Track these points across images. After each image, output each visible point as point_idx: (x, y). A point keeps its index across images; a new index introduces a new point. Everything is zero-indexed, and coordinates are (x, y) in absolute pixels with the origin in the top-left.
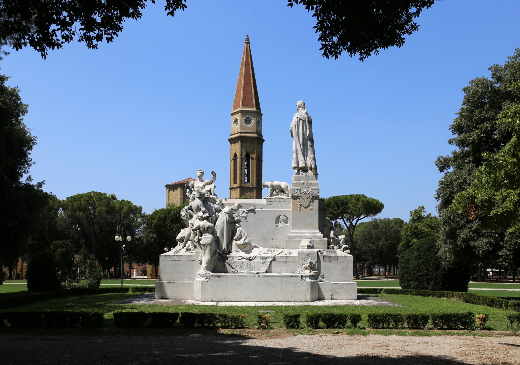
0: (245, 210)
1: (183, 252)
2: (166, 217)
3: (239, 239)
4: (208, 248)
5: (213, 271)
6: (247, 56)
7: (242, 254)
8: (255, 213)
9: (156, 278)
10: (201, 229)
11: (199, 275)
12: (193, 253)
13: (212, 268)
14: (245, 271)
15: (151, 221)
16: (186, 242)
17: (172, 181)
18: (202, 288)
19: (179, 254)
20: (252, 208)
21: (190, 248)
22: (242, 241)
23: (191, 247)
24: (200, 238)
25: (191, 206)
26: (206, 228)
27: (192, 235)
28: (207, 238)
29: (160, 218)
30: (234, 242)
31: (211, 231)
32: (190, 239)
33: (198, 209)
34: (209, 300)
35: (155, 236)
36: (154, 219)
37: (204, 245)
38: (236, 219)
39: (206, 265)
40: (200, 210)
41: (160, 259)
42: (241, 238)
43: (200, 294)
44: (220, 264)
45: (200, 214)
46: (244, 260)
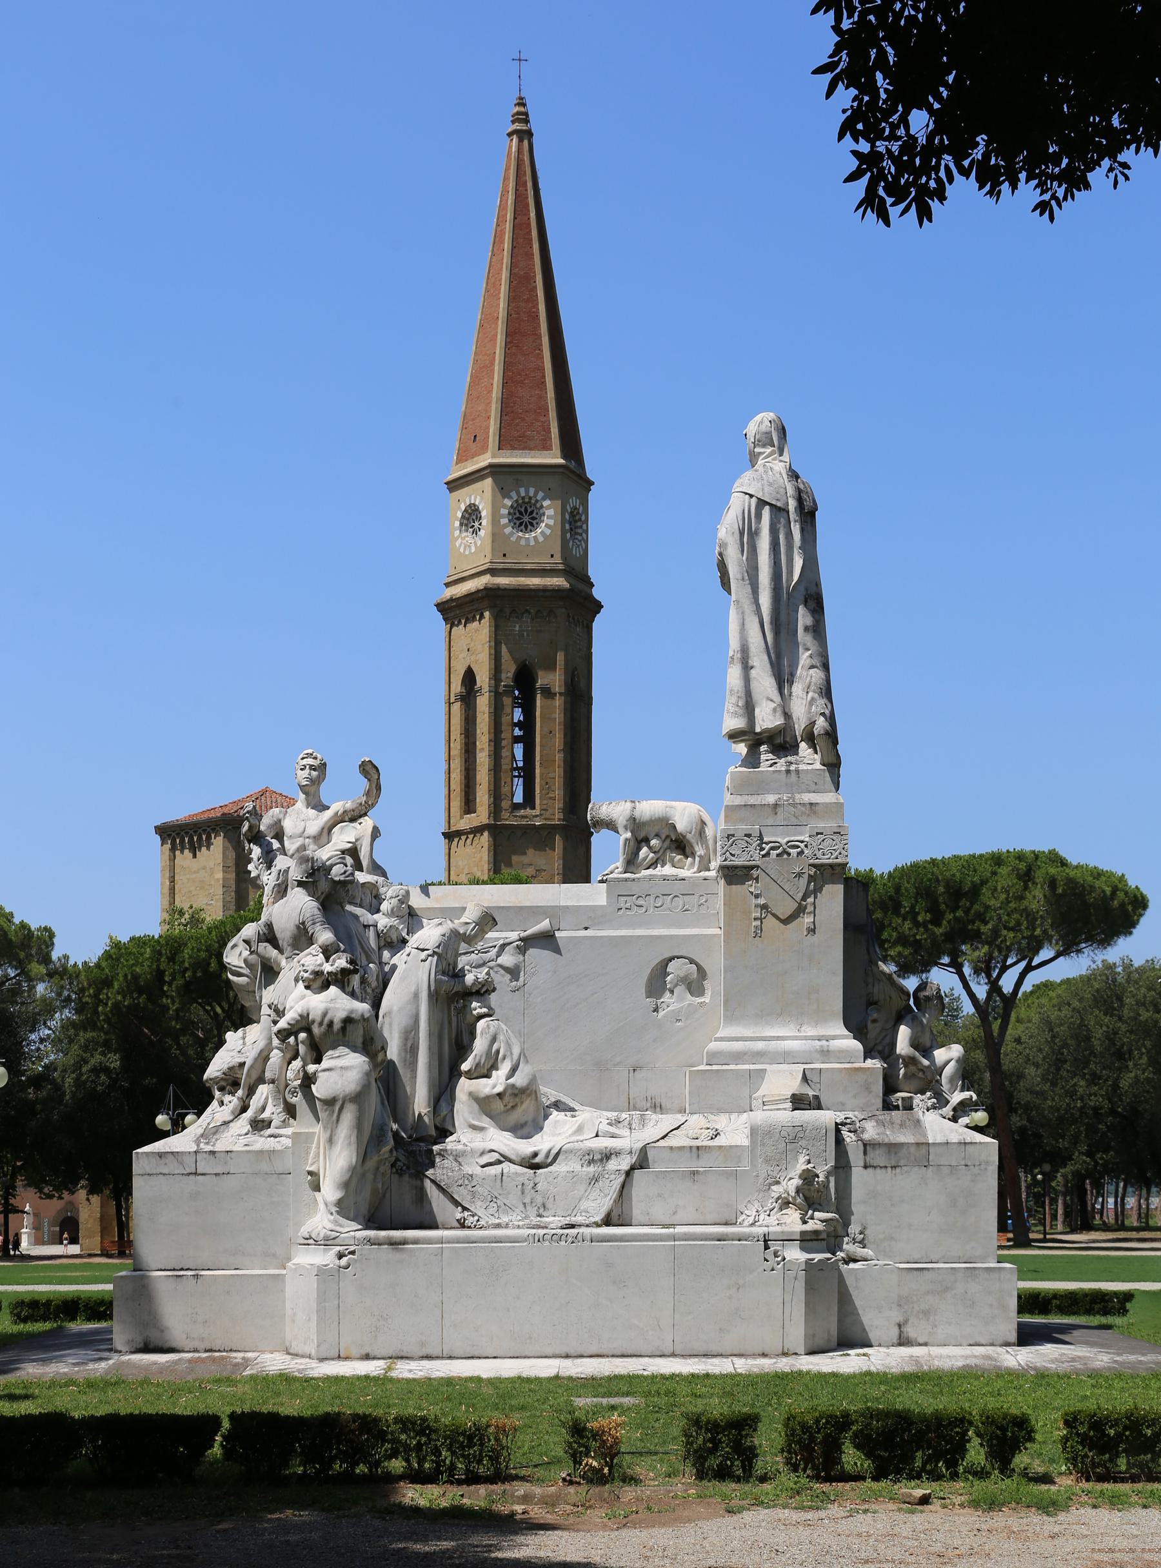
0: (513, 936)
1: (237, 1137)
2: (160, 974)
3: (484, 1071)
4: (348, 1117)
8: (557, 950)
10: (316, 1030)
11: (310, 1241)
12: (280, 1138)
13: (364, 1208)
14: (514, 1218)
15: (96, 996)
16: (251, 1091)
19: (220, 1147)
20: (544, 925)
21: (266, 1115)
22: (497, 1082)
23: (273, 1111)
24: (311, 1068)
25: (269, 926)
26: (337, 1026)
27: (276, 1056)
28: (343, 1070)
29: (136, 977)
30: (464, 1086)
32: (268, 1075)
33: (303, 938)
34: (355, 1352)
35: (114, 1061)
36: (107, 983)
37: (330, 1102)
38: (469, 978)
39: (338, 1195)
40: (310, 941)
41: (136, 1169)
42: (494, 1067)
43: (313, 1325)
45: (311, 959)
46: (507, 1167)
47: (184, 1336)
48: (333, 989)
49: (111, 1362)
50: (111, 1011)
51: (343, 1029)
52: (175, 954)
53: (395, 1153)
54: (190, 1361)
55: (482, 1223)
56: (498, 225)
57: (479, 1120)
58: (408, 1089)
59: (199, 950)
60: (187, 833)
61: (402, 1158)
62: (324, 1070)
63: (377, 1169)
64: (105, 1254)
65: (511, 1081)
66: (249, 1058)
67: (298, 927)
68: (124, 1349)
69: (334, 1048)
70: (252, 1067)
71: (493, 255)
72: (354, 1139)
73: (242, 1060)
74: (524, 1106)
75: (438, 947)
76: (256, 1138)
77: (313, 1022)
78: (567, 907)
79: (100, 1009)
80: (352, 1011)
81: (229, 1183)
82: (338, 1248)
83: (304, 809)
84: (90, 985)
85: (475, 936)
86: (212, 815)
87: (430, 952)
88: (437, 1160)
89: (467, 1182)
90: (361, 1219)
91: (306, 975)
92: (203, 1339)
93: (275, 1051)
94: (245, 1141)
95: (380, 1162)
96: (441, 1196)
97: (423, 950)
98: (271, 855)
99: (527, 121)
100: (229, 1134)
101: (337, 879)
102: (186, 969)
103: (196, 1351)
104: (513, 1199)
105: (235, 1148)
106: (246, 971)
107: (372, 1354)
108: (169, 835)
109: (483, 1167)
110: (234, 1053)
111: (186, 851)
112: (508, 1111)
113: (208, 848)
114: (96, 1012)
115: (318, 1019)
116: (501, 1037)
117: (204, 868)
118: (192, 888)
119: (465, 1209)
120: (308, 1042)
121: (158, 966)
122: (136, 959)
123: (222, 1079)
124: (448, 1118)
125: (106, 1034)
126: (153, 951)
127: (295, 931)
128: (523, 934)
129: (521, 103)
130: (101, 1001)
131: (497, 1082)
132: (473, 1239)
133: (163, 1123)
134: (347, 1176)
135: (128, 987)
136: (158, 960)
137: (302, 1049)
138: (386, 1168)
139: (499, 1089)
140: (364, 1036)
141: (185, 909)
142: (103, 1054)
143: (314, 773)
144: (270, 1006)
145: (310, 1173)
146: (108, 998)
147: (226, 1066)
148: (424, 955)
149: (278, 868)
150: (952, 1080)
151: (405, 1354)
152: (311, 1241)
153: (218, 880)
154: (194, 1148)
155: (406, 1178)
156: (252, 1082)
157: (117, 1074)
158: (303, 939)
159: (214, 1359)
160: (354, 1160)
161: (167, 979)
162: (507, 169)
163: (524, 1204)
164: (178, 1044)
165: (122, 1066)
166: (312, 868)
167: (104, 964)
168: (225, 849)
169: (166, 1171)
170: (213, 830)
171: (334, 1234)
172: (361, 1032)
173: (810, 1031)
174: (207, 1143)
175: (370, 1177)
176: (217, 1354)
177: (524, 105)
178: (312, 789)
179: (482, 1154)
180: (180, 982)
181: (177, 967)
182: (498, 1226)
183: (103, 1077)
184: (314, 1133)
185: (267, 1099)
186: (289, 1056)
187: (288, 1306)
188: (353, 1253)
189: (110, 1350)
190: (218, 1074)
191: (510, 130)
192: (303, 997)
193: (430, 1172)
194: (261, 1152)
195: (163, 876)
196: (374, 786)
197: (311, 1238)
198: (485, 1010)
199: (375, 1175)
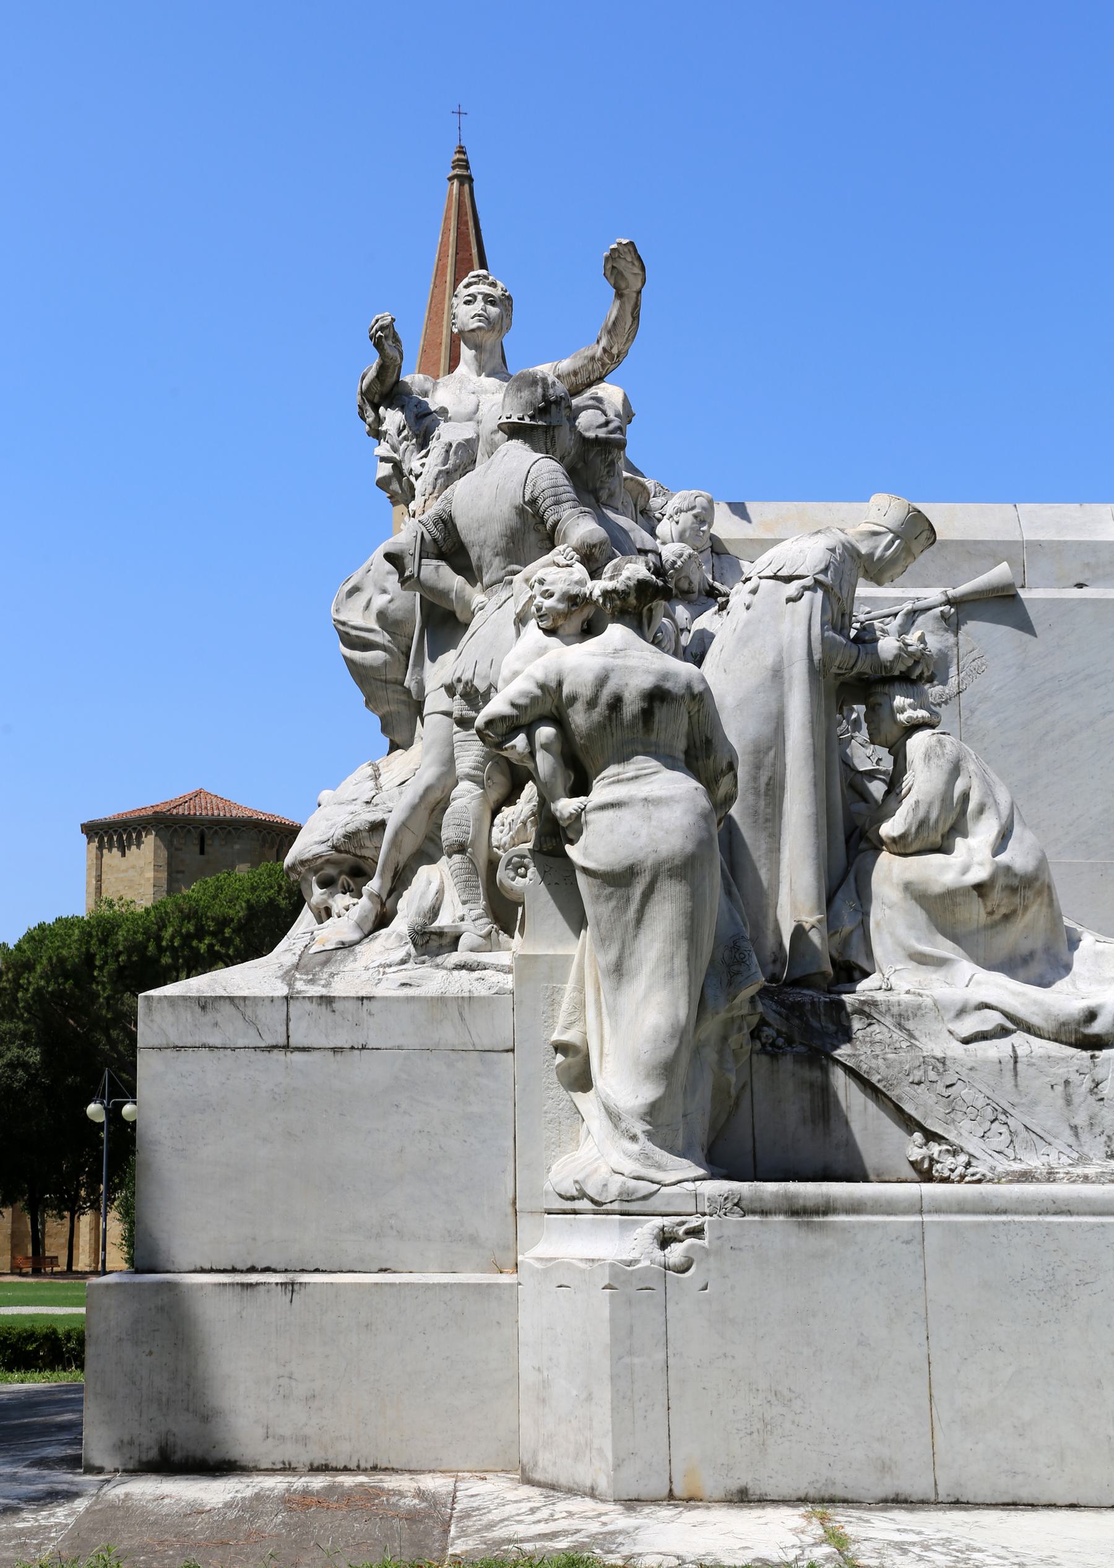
0: (933, 594)
1: (379, 967)
2: (89, 958)
3: (939, 835)
4: (666, 913)
5: (719, 1163)
6: (461, 236)
7: (974, 982)
8: (1025, 625)
9: (37, 1272)
10: (579, 719)
11: (579, 1203)
12: (492, 970)
13: (701, 1134)
14: (1054, 1157)
15: (16, 981)
16: (400, 880)
17: (112, 807)
18: (623, 1341)
19: (340, 988)
20: (999, 573)
21: (444, 921)
22: (971, 859)
23: (459, 912)
24: (566, 806)
25: (446, 523)
26: (631, 707)
27: (466, 798)
28: (640, 810)
29: (62, 961)
30: (889, 873)
31: (675, 726)
32: (448, 834)
33: (532, 532)
34: (711, 1484)
35: (34, 1055)
36: (28, 966)
37: (617, 879)
38: (888, 646)
39: (649, 1093)
40: (549, 540)
41: (145, 1034)
42: (958, 828)
43: (602, 1414)
44: (781, 1089)
45: (558, 573)
46: (1019, 1039)
47: (260, 1432)
48: (616, 633)
49: (81, 1505)
50: (32, 998)
51: (647, 715)
52: (108, 936)
53: (760, 1008)
54: (288, 1501)
55: (980, 1168)
56: (439, 260)
57: (934, 946)
58: (764, 874)
59: (135, 933)
60: (115, 831)
61: (772, 1018)
62: (603, 807)
63: (724, 1039)
64: (16, 1270)
65: (1003, 858)
66: (395, 808)
67: (520, 511)
68: (108, 1463)
69: (623, 758)
70: (404, 825)
71: (435, 286)
72: (680, 963)
73: (377, 816)
74: (1029, 916)
75: (825, 571)
76: (425, 970)
77: (573, 699)
78: (1039, 544)
79: (20, 995)
80: (665, 676)
81: (366, 1071)
82: (658, 1221)
83: (474, 377)
84: (8, 969)
85: (893, 561)
86: (143, 813)
87: (808, 582)
88: (857, 1024)
89: (932, 1076)
90: (701, 1155)
91: (548, 603)
92: (304, 1440)
93: (464, 785)
94: (402, 977)
95: (729, 1023)
96: (872, 1106)
97: (788, 579)
98: (427, 421)
99: (467, 168)
100: (357, 965)
101: (591, 434)
102: (120, 953)
103: (287, 1469)
104: (1047, 1115)
105: (378, 992)
106: (382, 638)
107: (755, 1490)
108: (97, 834)
109: (966, 1041)
110: (358, 807)
111: (115, 850)
112: (993, 925)
113: (138, 847)
114: (15, 1000)
115: (586, 692)
116: (970, 766)
117: (133, 867)
118: (121, 888)
119: (931, 1136)
120: (557, 747)
121: (88, 949)
122: (63, 941)
123: (328, 862)
124: (856, 940)
125: (25, 1023)
126: (83, 932)
127: (514, 520)
128: (951, 592)
129: (461, 151)
130: (21, 986)
131: (971, 859)
132: (996, 1205)
133: (96, 1113)
134: (669, 1050)
135: (52, 971)
136: (88, 942)
137: (544, 763)
138: (739, 1039)
139: (978, 874)
140: (690, 736)
141: (116, 900)
142: (21, 1047)
143: (493, 311)
144: (450, 690)
145: (560, 1048)
146: (29, 983)
147: (339, 832)
148: (793, 588)
149: (445, 439)
151: (839, 1492)
152: (585, 1204)
153: (148, 879)
154: (283, 991)
155: (787, 1064)
156: (402, 858)
157: (37, 1070)
158: (532, 538)
159: (347, 1496)
160: (683, 1013)
161: (97, 963)
162: (449, 209)
163: (1074, 1128)
164: (108, 1036)
165: (43, 1061)
166: (545, 397)
167: (25, 947)
168: (156, 848)
169: (216, 1041)
170: (144, 828)
171: (645, 1187)
172: (683, 725)
174: (312, 982)
175: (710, 1055)
176: (348, 1481)
177: (464, 153)
178: (489, 339)
179: (962, 1012)
180: (112, 966)
181: (109, 951)
182: (1025, 1177)
183: (20, 1072)
184: (568, 959)
185: (440, 892)
186: (495, 795)
187: (526, 1363)
188: (696, 1232)
189: (75, 1463)
190: (322, 848)
191: (450, 175)
192: (542, 651)
193: (843, 1052)
194: (441, 1001)
195: (89, 875)
196: (629, 309)
197: (583, 1195)
198: (921, 713)
199: (721, 1052)
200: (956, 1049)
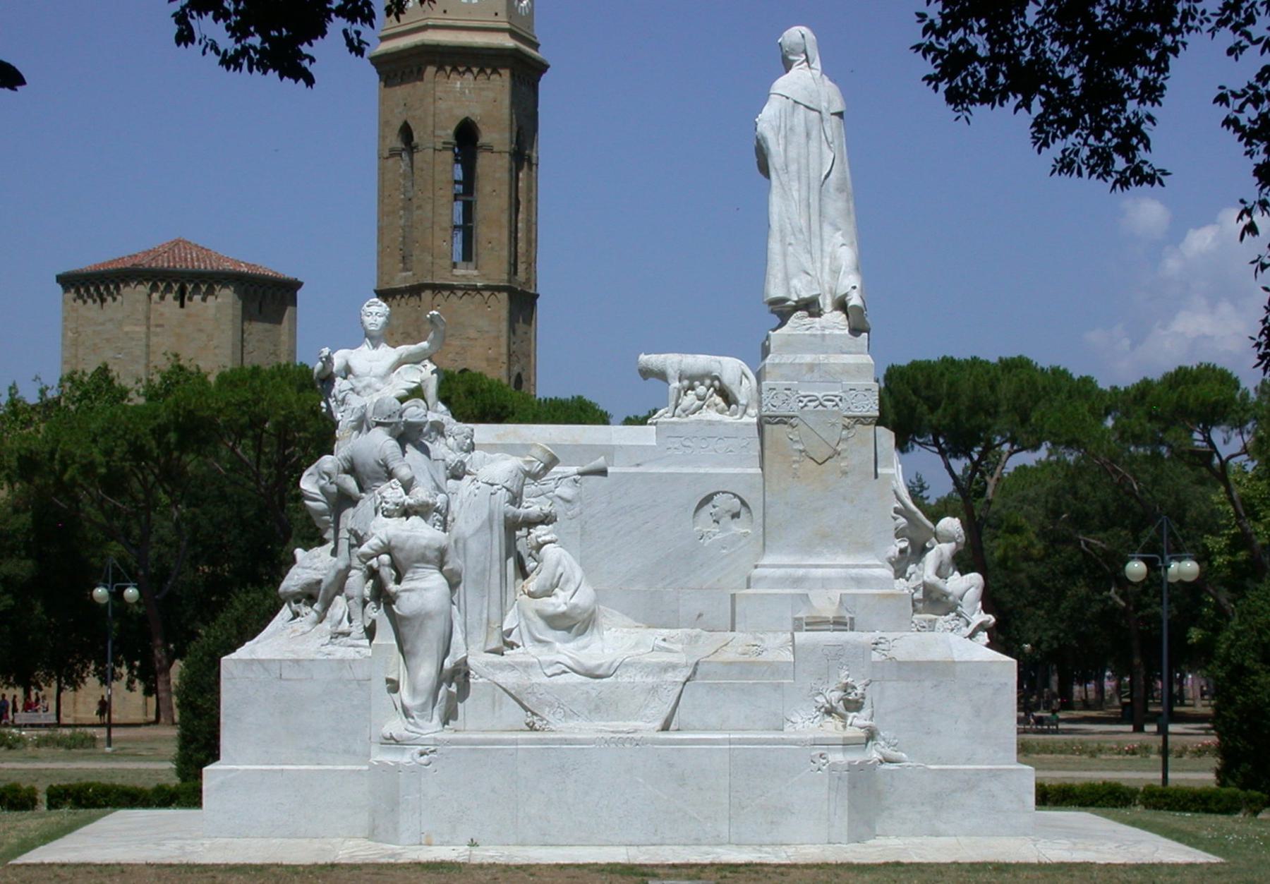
0: (574, 469)
16: (328, 604)
20: (600, 462)
108: (73, 285)
117: (111, 320)
119: (533, 714)
150: (973, 604)
170: (123, 281)
173: (842, 559)
194: (342, 661)
200: (545, 680)
